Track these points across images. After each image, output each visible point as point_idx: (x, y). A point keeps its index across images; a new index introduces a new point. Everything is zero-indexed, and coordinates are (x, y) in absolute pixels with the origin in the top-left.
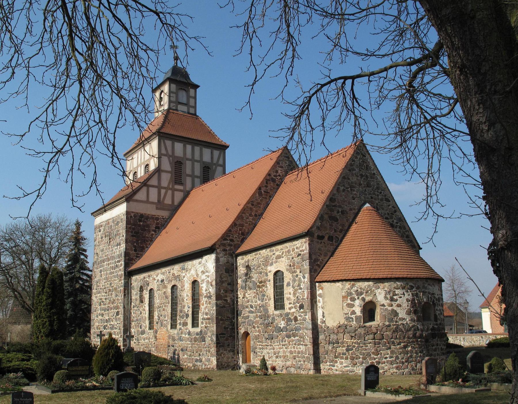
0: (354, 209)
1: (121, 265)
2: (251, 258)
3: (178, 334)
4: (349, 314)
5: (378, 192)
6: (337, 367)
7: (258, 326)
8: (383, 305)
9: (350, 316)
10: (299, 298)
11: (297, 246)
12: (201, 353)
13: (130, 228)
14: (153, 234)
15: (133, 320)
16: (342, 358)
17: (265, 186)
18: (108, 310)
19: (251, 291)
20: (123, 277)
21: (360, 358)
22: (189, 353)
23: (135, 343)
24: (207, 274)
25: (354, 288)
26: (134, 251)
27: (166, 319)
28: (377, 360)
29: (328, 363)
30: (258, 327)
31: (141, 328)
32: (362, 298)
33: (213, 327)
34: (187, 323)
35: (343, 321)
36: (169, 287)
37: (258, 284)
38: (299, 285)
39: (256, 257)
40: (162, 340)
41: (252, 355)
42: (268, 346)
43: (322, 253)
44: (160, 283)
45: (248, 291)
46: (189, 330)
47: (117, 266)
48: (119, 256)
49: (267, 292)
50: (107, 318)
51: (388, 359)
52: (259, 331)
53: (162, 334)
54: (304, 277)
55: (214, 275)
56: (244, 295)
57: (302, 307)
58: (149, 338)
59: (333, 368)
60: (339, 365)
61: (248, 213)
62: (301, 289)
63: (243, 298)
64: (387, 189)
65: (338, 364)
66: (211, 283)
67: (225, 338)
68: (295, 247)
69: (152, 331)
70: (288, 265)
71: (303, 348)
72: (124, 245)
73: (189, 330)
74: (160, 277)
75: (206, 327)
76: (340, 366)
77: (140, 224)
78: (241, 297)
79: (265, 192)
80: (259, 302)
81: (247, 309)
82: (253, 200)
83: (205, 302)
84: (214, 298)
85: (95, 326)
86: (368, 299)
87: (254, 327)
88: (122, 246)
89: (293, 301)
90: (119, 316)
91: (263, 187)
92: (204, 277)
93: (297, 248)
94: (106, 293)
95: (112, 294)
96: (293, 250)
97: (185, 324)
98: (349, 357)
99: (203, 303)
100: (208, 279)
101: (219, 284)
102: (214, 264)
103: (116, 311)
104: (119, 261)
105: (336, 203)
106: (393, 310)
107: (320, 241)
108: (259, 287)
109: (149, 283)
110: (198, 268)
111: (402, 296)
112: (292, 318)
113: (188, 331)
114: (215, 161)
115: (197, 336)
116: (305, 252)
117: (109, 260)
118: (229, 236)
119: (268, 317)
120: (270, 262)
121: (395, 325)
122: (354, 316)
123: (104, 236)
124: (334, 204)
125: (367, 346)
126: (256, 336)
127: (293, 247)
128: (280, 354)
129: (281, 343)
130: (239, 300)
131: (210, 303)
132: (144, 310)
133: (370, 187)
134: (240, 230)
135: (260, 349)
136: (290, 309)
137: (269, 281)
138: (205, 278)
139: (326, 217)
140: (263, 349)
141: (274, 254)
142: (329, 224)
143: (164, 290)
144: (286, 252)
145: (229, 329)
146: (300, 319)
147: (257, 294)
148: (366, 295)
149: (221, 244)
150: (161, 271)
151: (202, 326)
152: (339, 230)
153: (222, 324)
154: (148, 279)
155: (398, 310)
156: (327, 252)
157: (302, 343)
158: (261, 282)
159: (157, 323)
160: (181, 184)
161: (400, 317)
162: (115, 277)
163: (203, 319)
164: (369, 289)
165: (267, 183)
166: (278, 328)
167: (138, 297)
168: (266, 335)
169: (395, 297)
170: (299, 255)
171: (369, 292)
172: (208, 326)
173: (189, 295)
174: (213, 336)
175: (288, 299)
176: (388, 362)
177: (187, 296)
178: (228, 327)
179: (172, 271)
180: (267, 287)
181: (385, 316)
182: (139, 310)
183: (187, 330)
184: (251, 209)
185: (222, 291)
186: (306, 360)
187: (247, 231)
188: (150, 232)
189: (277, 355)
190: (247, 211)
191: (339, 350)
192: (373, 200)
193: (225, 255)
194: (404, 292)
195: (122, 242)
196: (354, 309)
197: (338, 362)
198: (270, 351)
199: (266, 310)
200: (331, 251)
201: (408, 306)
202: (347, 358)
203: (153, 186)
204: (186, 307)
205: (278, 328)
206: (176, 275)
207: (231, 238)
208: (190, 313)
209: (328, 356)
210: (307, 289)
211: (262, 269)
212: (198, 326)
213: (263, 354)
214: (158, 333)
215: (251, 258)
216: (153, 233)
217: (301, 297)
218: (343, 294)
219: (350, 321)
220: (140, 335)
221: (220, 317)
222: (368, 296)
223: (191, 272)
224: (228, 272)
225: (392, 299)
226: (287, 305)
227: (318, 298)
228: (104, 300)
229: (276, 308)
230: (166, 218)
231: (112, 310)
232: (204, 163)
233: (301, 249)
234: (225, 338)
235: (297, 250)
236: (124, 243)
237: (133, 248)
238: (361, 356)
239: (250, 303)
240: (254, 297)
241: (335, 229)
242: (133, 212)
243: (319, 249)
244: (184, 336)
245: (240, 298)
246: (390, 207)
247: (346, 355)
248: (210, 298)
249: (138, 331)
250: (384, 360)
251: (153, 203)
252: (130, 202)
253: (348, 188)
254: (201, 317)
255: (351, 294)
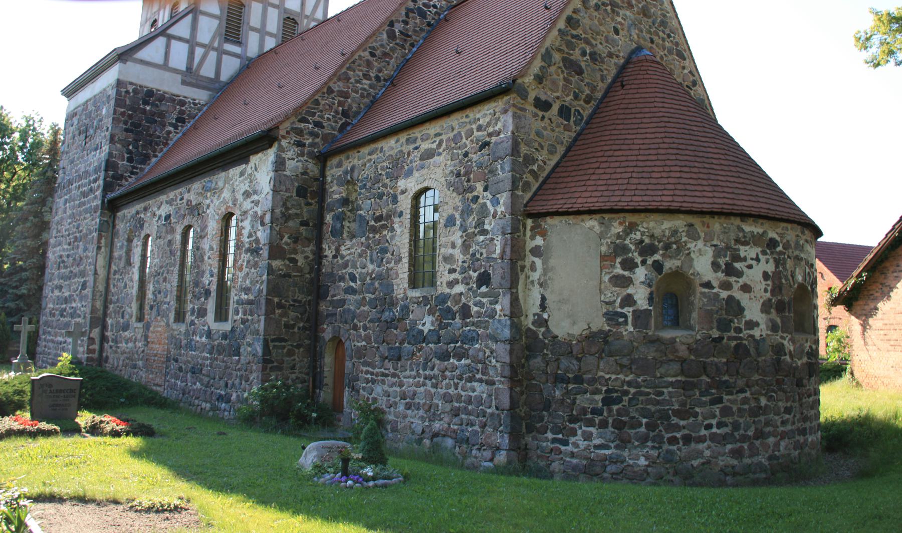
0: (617, 56)
1: (99, 186)
2: (360, 162)
3: (187, 333)
4: (617, 304)
5: (664, 32)
6: (576, 445)
7: (365, 326)
8: (708, 285)
9: (619, 310)
10: (478, 256)
11: (481, 122)
12: (230, 382)
13: (123, 114)
14: (169, 132)
15: (111, 299)
16: (590, 423)
17: (403, 21)
18: (70, 279)
19: (354, 241)
20: (99, 211)
21: (640, 425)
22: (206, 379)
23: (111, 347)
24: (255, 197)
25: (633, 236)
26: (128, 161)
27: (167, 300)
28: (686, 432)
29: (550, 435)
30: (365, 328)
31: (123, 317)
32: (655, 261)
33: (259, 321)
34: (206, 310)
35: (600, 323)
36: (179, 230)
37: (372, 223)
38: (480, 223)
39: (371, 160)
40: (157, 346)
41: (346, 394)
42: (387, 375)
43: (543, 144)
44: (163, 222)
45: (348, 243)
46: (209, 327)
47: (91, 190)
48: (97, 170)
49: (393, 243)
50: (67, 294)
51: (714, 430)
52: (367, 339)
53: (158, 332)
54: (496, 202)
55: (270, 197)
56: (338, 250)
57: (484, 279)
58: (136, 339)
59: (563, 448)
60: (580, 443)
61: (362, 71)
62: (484, 232)
63: (335, 257)
64: (680, 31)
65: (578, 439)
66: (262, 218)
67: (285, 351)
68: (474, 127)
69: (140, 325)
70: (452, 172)
71: (480, 389)
72: (107, 147)
73: (209, 327)
74: (164, 210)
75: (244, 322)
76: (583, 444)
77: (145, 110)
78: (331, 256)
79: (401, 32)
80: (371, 267)
81: (342, 284)
82: (374, 44)
83: (245, 263)
84: (265, 253)
85: (48, 310)
86: (670, 265)
87: (355, 328)
88: (104, 148)
89: (460, 263)
90: (86, 291)
91: (398, 21)
92: (247, 205)
93: (480, 128)
94: (69, 244)
95: (78, 247)
96: (470, 133)
97: (202, 313)
98: (611, 421)
99: (242, 265)
100: (256, 209)
101: (280, 220)
102: (272, 174)
103: (82, 280)
104: (95, 181)
105: (579, 31)
106: (731, 298)
107: (541, 114)
108: (374, 230)
109: (143, 224)
110: (237, 186)
111: (754, 263)
112: (455, 309)
113: (206, 328)
114: (308, 11)
115: (223, 342)
116: (502, 136)
117: (80, 178)
118: (314, 114)
119: (393, 304)
120: (406, 167)
121: (735, 338)
122: (631, 309)
123: (77, 133)
124: (574, 32)
125: (662, 393)
126: (359, 349)
127: (468, 127)
128: (417, 401)
129: (421, 372)
130: (324, 261)
131: (255, 266)
132: (132, 280)
133: (650, 17)
134: (340, 104)
135: (367, 381)
136: (451, 284)
137: (401, 215)
138: (249, 208)
139: (557, 57)
140: (373, 381)
141: (416, 148)
142: (561, 76)
143: (169, 237)
144: (448, 140)
145: (296, 330)
146: (478, 312)
147: (368, 247)
148: (663, 255)
149: (292, 129)
150: (168, 197)
151: (236, 317)
152: (583, 97)
153: (281, 315)
154: (142, 216)
155: (744, 299)
156: (555, 144)
157: (478, 376)
158: (379, 219)
159: (152, 308)
160: (239, 43)
161: (747, 318)
162: (86, 211)
163: (238, 302)
164: (673, 239)
165: (407, 15)
166: (415, 333)
167: (123, 252)
168: (383, 348)
169: (737, 265)
170: (486, 144)
171: (674, 246)
172: (248, 320)
173: (215, 247)
174: (256, 343)
175: (448, 259)
176: (713, 437)
177: (211, 248)
178: (294, 325)
179: (186, 196)
180: (393, 230)
181: (710, 313)
182: (123, 279)
183: (204, 326)
184: (369, 64)
185: (286, 239)
186: (489, 423)
187: (354, 109)
188: (164, 126)
189: (408, 400)
190: (359, 66)
191: (583, 401)
192: (654, 46)
193: (299, 155)
194: (757, 255)
195: (104, 141)
196: (630, 291)
197: (579, 432)
198: (391, 390)
199: (389, 288)
200: (565, 142)
201: (766, 291)
202: (603, 425)
203: (180, 39)
204: (207, 275)
205: (415, 333)
206: (194, 203)
207: (316, 118)
208: (214, 288)
209: (550, 415)
210: (504, 234)
211: (385, 186)
212: (226, 320)
213: (373, 395)
214: (151, 329)
215: (360, 162)
216: (171, 129)
217: (485, 255)
218: (604, 249)
219: (619, 324)
220: (121, 332)
221: (276, 300)
222: (671, 257)
223: (223, 196)
224: (305, 197)
225: (730, 271)
226: (444, 276)
227: (530, 258)
228: (65, 259)
229: (413, 283)
230: (199, 104)
231: (76, 280)
232: (286, 11)
233: (491, 130)
234: (285, 351)
235: (480, 133)
236: (108, 142)
237: (126, 156)
238: (644, 421)
239: (349, 270)
240: (360, 256)
241: (575, 92)
242: (131, 83)
243: (538, 134)
244: (198, 338)
245: (326, 256)
246: (686, 71)
247: (601, 414)
248: (257, 252)
249: (118, 322)
250: (703, 432)
251: (176, 71)
252: (128, 63)
253: (607, 5)
254: (236, 298)
255: (625, 249)
